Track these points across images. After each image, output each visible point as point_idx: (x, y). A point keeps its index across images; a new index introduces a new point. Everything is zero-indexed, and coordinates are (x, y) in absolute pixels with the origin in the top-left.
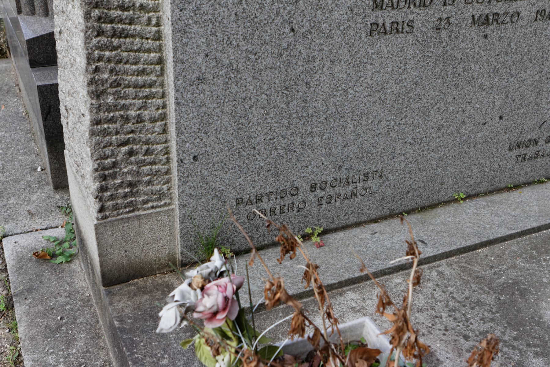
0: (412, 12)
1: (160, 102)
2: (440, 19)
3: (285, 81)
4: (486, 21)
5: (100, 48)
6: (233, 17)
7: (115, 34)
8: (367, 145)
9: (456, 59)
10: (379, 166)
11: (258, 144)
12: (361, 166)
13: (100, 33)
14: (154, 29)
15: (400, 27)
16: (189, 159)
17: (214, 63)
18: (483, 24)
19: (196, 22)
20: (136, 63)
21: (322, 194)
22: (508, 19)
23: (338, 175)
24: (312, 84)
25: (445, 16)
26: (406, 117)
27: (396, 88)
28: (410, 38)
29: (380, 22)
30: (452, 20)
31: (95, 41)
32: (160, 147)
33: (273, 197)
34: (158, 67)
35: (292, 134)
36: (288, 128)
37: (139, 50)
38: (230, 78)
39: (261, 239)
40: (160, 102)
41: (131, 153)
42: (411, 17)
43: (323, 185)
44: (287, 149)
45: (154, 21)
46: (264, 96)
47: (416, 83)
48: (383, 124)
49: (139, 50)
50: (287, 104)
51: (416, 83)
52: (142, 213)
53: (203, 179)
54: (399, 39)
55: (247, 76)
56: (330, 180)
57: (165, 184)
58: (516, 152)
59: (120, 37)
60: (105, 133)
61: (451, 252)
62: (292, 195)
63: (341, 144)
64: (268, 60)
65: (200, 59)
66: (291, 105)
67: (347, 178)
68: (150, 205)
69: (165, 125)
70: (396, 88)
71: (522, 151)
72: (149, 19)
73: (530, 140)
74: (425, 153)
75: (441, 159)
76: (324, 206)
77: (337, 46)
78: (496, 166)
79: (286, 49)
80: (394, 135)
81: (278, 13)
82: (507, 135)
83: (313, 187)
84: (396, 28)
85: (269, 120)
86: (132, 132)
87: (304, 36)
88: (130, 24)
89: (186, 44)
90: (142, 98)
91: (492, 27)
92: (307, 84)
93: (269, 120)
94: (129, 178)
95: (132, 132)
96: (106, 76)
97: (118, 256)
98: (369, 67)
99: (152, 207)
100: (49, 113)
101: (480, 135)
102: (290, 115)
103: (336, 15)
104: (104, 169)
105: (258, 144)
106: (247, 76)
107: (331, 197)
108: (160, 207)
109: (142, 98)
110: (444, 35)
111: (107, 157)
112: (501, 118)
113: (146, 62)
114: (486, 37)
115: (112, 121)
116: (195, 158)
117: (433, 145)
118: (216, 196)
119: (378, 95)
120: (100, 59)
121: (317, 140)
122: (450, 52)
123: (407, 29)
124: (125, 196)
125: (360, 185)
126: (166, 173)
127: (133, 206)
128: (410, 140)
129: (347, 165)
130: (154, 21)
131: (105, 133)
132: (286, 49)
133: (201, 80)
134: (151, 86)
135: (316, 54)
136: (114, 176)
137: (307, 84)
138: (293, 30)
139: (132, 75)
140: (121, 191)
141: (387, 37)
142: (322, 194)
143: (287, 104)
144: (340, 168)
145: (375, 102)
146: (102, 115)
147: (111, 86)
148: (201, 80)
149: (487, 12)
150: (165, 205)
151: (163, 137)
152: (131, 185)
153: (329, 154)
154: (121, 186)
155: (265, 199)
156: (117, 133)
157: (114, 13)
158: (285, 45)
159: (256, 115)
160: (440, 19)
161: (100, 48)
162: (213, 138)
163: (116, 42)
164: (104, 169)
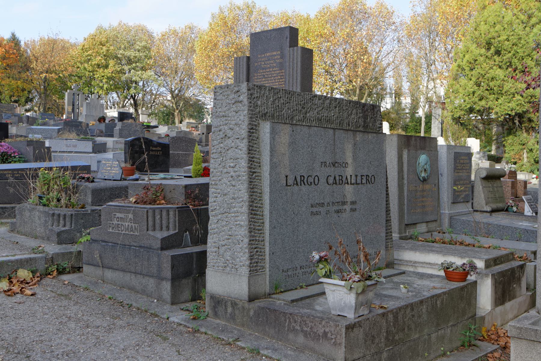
13: (252, 214)
110: (328, 215)
131: (252, 244)
146: (252, 238)
152: (257, 263)
163: (254, 216)
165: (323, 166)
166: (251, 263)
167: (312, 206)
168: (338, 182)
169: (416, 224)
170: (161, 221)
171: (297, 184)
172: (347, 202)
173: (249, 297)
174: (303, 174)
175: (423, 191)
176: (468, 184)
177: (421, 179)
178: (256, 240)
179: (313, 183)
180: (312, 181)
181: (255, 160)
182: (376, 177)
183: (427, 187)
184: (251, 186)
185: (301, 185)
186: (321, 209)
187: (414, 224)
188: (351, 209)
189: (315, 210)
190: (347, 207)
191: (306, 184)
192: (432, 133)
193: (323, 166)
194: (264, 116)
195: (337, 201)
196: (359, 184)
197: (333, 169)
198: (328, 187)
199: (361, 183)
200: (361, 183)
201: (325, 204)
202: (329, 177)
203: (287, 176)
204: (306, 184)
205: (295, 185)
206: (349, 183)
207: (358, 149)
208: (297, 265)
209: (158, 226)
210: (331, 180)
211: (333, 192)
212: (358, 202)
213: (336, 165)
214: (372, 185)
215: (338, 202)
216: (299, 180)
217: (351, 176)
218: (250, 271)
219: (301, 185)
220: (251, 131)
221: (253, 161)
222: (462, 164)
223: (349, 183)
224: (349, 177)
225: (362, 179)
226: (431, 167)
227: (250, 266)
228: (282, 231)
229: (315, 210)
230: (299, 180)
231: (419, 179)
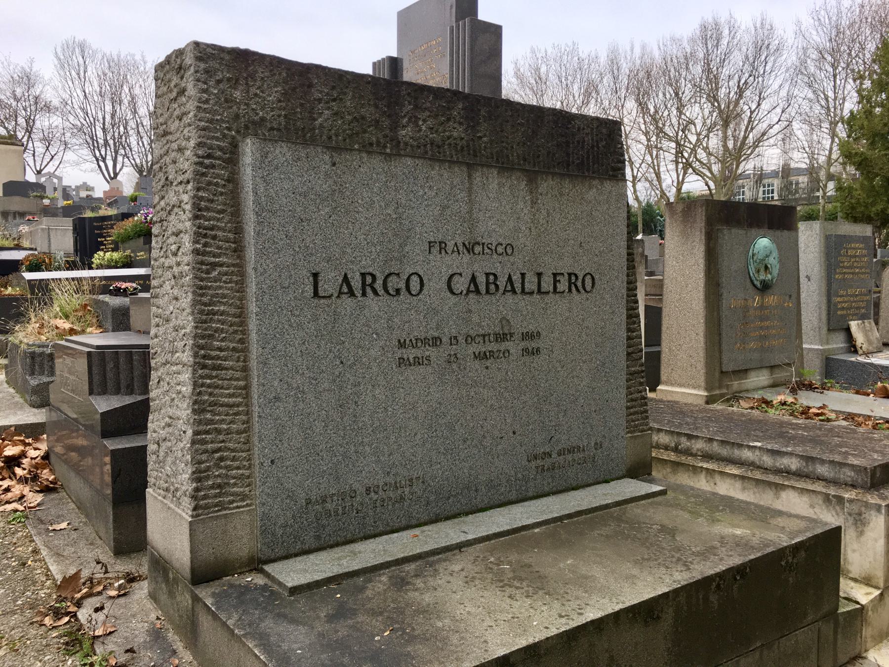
0: (428, 350)
1: (244, 418)
2: (450, 355)
3: (339, 400)
4: (485, 357)
5: (202, 377)
6: (299, 353)
7: (215, 368)
8: (408, 454)
9: (468, 385)
10: (421, 474)
11: (321, 451)
12: (406, 474)
13: (204, 367)
14: (241, 364)
15: (421, 361)
16: (267, 463)
17: (286, 386)
18: (483, 359)
19: (273, 357)
20: (228, 389)
21: (375, 497)
22: (501, 355)
23: (388, 479)
24: (359, 403)
25: (452, 353)
26: (436, 430)
27: (424, 407)
28: (429, 369)
29: (405, 357)
30: (458, 356)
31: (200, 372)
32: (244, 455)
33: (335, 498)
34: (244, 392)
35: (347, 443)
36: (344, 438)
37: (230, 379)
38: (298, 398)
39: (327, 538)
40: (244, 418)
41: (221, 459)
42: (427, 353)
43: (376, 489)
44: (345, 456)
45: (242, 358)
46: (324, 412)
47: (440, 403)
48: (419, 436)
49: (230, 379)
50: (342, 419)
51: (440, 403)
52: (228, 512)
53: (278, 480)
54: (421, 369)
55: (310, 396)
56: (381, 484)
57: (247, 486)
58: (533, 464)
59: (218, 370)
60: (204, 442)
61: (487, 536)
62: (351, 497)
63: (387, 453)
64: (326, 384)
65: (276, 383)
66: (345, 419)
67: (396, 483)
68: (235, 505)
69: (249, 436)
70: (424, 407)
71: (539, 462)
72: (239, 357)
73: (544, 453)
74: (457, 462)
75: (471, 468)
76: (378, 509)
77: (375, 374)
78: (520, 475)
79: (338, 377)
80: (428, 446)
81: (330, 351)
82: (523, 448)
83: (368, 490)
84: (418, 361)
85: (329, 431)
86: (223, 441)
87: (351, 367)
88: (225, 360)
89: (266, 372)
90: (232, 415)
91: (490, 361)
92: (356, 403)
93: (329, 431)
94: (219, 481)
95: (223, 441)
96: (206, 398)
97: (207, 553)
98: (401, 390)
99: (238, 507)
100: (119, 475)
101: (500, 447)
102: (345, 427)
103: (372, 352)
104: (200, 472)
105: (321, 451)
106: (310, 396)
107: (383, 501)
108: (243, 507)
109: (232, 415)
110: (455, 366)
111: (203, 462)
112: (514, 433)
113: (236, 388)
114: (487, 368)
115: (207, 432)
116: (272, 462)
117: (463, 456)
118: (289, 496)
119: (411, 412)
120: (203, 385)
121: (367, 448)
122: (462, 379)
123: (426, 362)
124: (215, 496)
125: (407, 490)
126: (248, 477)
127: (222, 506)
128: (442, 450)
129: (393, 471)
130: (242, 358)
131: (204, 442)
132: (338, 377)
133: (277, 399)
134: (238, 406)
135: (360, 380)
136: (208, 478)
137: (356, 403)
138: (342, 363)
139: (226, 397)
140: (213, 491)
141: (412, 368)
142: (375, 497)
143: (342, 419)
144: (388, 473)
145: (409, 418)
146: (201, 428)
147: (210, 406)
148: (277, 399)
149: (484, 350)
150: (247, 505)
151: (246, 447)
152: (219, 486)
153: (378, 461)
154: (212, 487)
155: (329, 500)
156: (212, 442)
157: (213, 353)
158: (337, 373)
159: (319, 426)
160: (450, 355)
161: (202, 377)
162: (286, 445)
163: (214, 373)
164: (200, 472)
165: (436, 250)
166: (197, 490)
167: (402, 345)
168: (483, 288)
169: (746, 371)
170: (118, 374)
171: (351, 293)
172: (511, 335)
173: (193, 570)
174: (371, 270)
175: (762, 307)
176: (866, 295)
177: (758, 284)
178: (219, 431)
179: (404, 291)
180: (402, 285)
181: (220, 233)
182: (597, 277)
183: (771, 300)
184: (205, 299)
185: (364, 294)
186: (431, 352)
187: (739, 371)
188: (525, 350)
189: (411, 354)
190: (514, 347)
191: (381, 292)
192: (404, 75)
193: (436, 250)
194: (253, 127)
195: (481, 332)
196: (532, 293)
197: (466, 258)
198: (453, 299)
199: (539, 291)
200: (539, 291)
201: (445, 340)
202: (456, 278)
203: (315, 275)
204: (381, 292)
205: (471, 295)
206: (518, 289)
207: (544, 212)
208: (356, 486)
209: (110, 384)
210: (461, 284)
211: (470, 311)
212: (544, 333)
213: (478, 249)
214: (584, 295)
215: (484, 336)
216: (356, 283)
217: (523, 275)
218: (195, 509)
219: (364, 294)
220: (207, 161)
221: (214, 237)
222: (851, 256)
223: (518, 289)
224: (516, 278)
225: (556, 282)
226: (780, 261)
227: (194, 497)
228: (301, 406)
229: (411, 354)
230: (356, 283)
231: (754, 285)
